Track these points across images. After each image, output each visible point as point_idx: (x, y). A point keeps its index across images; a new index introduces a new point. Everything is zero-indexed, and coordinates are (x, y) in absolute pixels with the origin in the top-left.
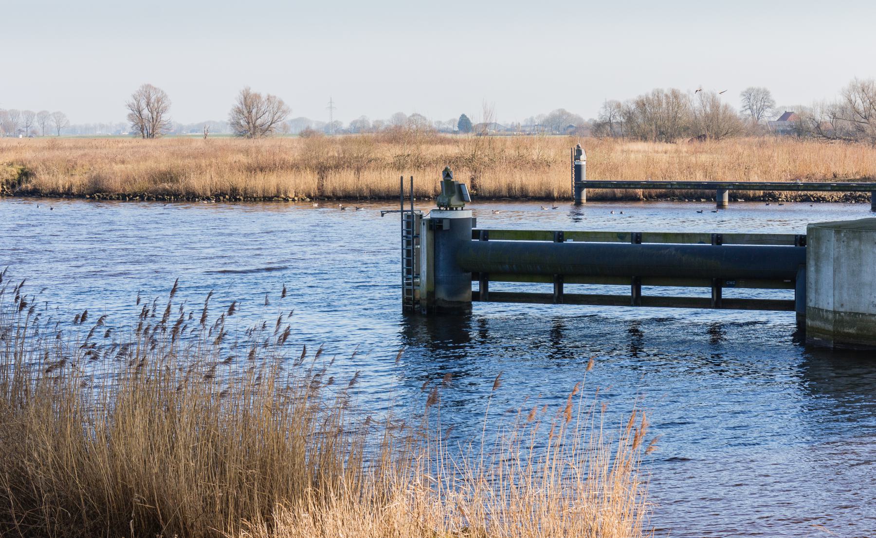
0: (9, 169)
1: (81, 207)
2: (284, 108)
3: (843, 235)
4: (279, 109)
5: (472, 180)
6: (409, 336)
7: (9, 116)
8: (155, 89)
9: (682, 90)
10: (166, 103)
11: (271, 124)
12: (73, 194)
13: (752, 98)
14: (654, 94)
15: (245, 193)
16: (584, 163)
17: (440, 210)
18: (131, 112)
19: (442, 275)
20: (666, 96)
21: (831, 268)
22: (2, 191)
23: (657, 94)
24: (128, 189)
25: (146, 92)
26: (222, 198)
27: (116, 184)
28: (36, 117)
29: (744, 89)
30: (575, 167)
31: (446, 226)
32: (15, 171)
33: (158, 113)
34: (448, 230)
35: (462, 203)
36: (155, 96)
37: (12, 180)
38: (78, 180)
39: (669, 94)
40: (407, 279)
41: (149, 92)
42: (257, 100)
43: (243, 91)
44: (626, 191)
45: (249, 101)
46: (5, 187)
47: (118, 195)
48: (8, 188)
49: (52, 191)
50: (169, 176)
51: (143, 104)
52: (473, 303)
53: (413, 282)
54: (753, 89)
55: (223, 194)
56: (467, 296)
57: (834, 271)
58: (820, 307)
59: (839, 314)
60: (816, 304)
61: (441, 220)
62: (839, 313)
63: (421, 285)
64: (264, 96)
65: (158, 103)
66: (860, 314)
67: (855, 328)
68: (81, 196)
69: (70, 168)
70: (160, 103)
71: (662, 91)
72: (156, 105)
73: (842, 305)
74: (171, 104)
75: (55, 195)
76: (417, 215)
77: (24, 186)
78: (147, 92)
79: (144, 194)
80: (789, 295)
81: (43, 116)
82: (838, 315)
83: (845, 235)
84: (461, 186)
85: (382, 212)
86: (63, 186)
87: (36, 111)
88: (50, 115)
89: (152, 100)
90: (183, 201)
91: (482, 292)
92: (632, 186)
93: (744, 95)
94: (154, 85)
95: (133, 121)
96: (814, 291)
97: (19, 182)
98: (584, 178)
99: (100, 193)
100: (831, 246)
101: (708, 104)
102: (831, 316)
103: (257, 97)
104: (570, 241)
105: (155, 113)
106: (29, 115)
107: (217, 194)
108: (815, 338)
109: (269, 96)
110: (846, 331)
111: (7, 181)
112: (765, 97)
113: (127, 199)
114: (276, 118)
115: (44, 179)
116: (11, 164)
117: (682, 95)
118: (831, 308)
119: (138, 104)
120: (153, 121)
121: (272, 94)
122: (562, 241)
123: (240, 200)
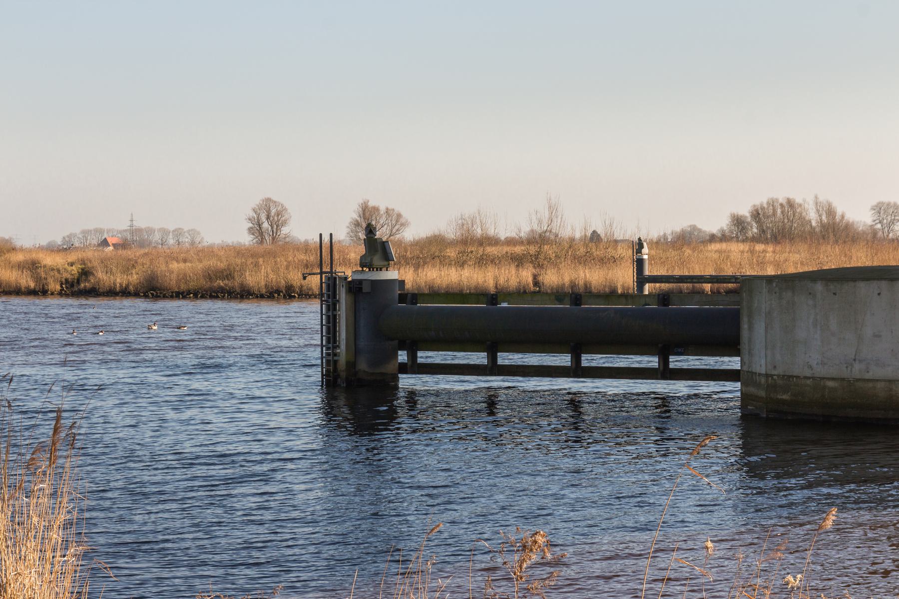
0: (70, 268)
1: (141, 304)
2: (402, 220)
3: (774, 285)
4: (397, 221)
5: (535, 277)
6: (329, 410)
7: (145, 234)
8: (275, 202)
9: (798, 200)
10: (286, 216)
11: (389, 237)
12: (129, 293)
13: (882, 212)
14: (768, 203)
15: (301, 291)
16: (646, 257)
17: (363, 270)
18: (251, 225)
19: (362, 343)
20: (781, 205)
21: (763, 325)
22: (61, 290)
23: (772, 203)
24: (183, 287)
25: (266, 205)
26: (276, 295)
27: (172, 282)
28: (171, 234)
29: (874, 203)
30: (636, 261)
31: (366, 288)
32: (75, 269)
33: (277, 226)
34: (369, 293)
35: (386, 263)
36: (275, 209)
37: (71, 279)
38: (134, 278)
39: (784, 202)
40: (328, 349)
41: (269, 206)
42: (376, 213)
43: (362, 204)
44: (693, 286)
45: (367, 215)
46: (64, 286)
47: (172, 293)
48: (67, 288)
49: (110, 290)
50: (227, 274)
51: (263, 217)
52: (400, 375)
53: (333, 351)
54: (883, 203)
55: (278, 292)
56: (391, 368)
57: (766, 328)
58: (754, 371)
59: (772, 378)
60: (749, 367)
61: (360, 282)
62: (772, 376)
63: (341, 354)
64: (382, 209)
65: (278, 216)
66: (795, 376)
67: (789, 394)
68: (136, 295)
69: (129, 266)
70: (280, 216)
71: (777, 200)
72: (276, 218)
73: (775, 367)
74: (291, 217)
75: (112, 293)
76: (340, 278)
77: (82, 285)
78: (267, 204)
79: (198, 291)
80: (733, 363)
81: (178, 232)
82: (770, 378)
83: (776, 285)
84: (386, 244)
85: (303, 274)
86: (120, 284)
87: (171, 228)
88: (185, 232)
89: (273, 214)
90: (237, 298)
91: (410, 363)
92: (694, 280)
93: (874, 210)
94: (274, 198)
95: (253, 234)
96: (747, 353)
97: (78, 282)
98: (647, 272)
99: (154, 291)
100: (763, 301)
101: (824, 213)
102: (763, 380)
103: (376, 209)
104: (505, 305)
105: (275, 227)
106: (165, 232)
107: (272, 292)
108: (749, 407)
109: (387, 209)
110: (779, 397)
111: (66, 280)
112: (895, 211)
113: (181, 297)
114: (394, 230)
115: (102, 277)
116: (72, 264)
117: (798, 204)
118: (763, 372)
119: (258, 218)
120: (273, 235)
121: (390, 207)
122: (496, 304)
123: (294, 297)
